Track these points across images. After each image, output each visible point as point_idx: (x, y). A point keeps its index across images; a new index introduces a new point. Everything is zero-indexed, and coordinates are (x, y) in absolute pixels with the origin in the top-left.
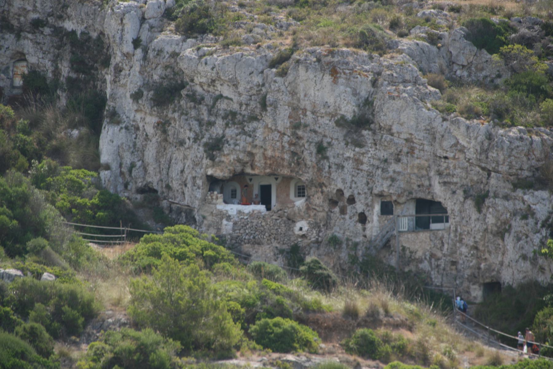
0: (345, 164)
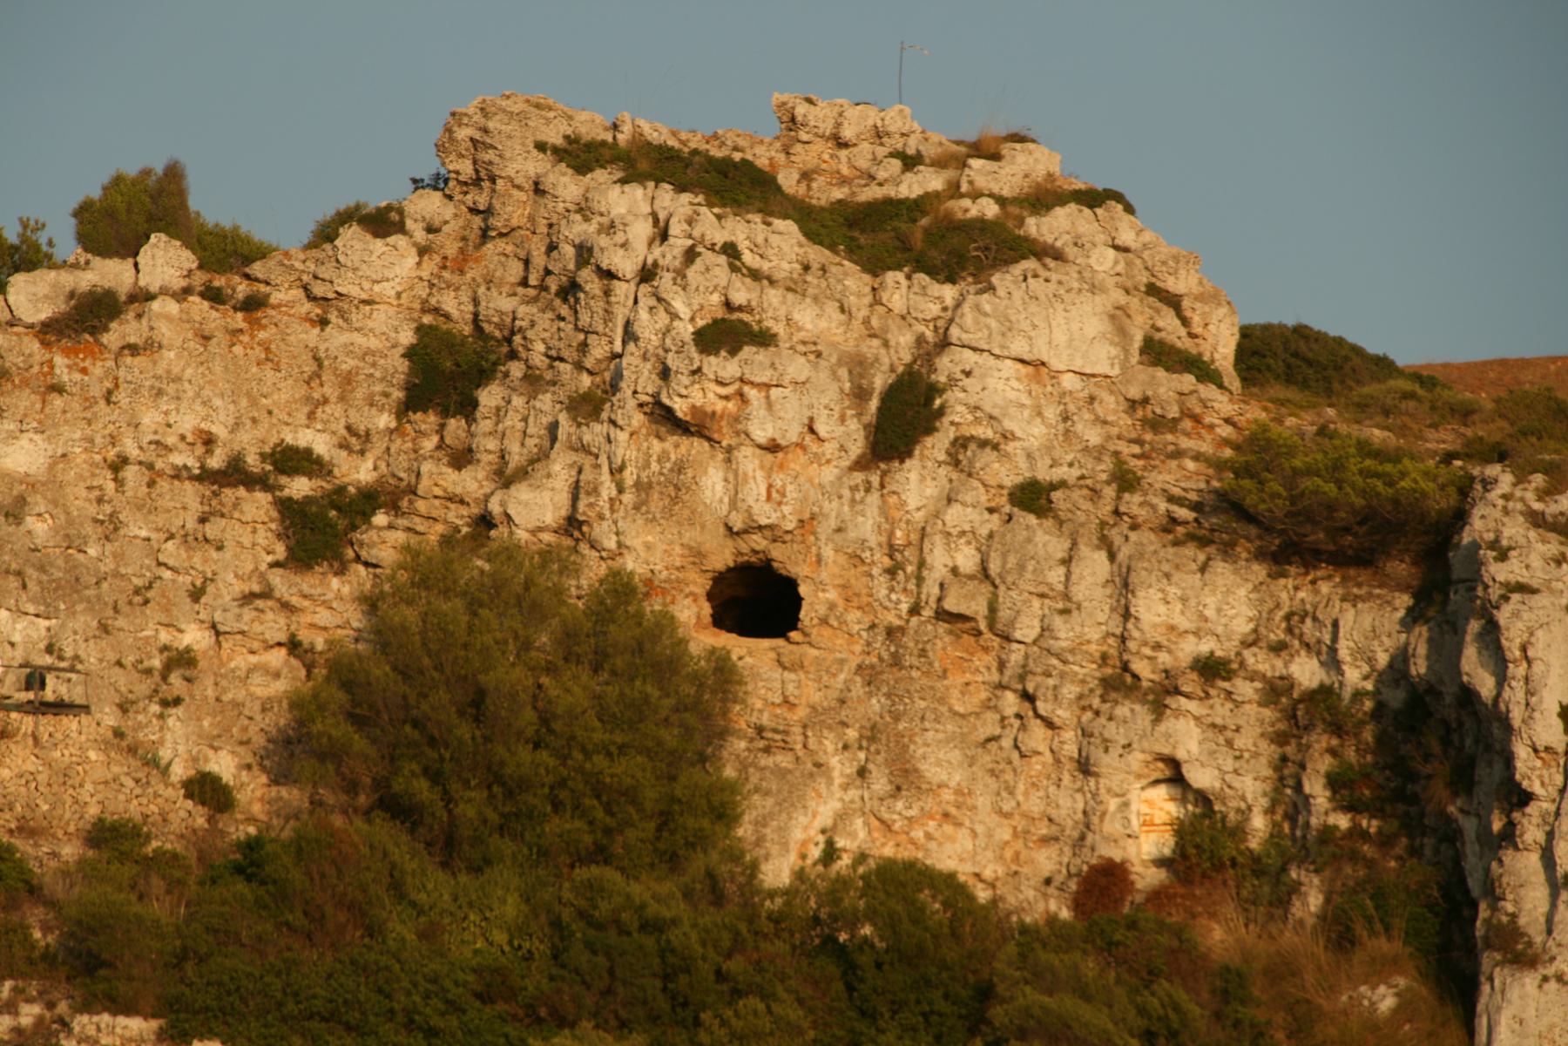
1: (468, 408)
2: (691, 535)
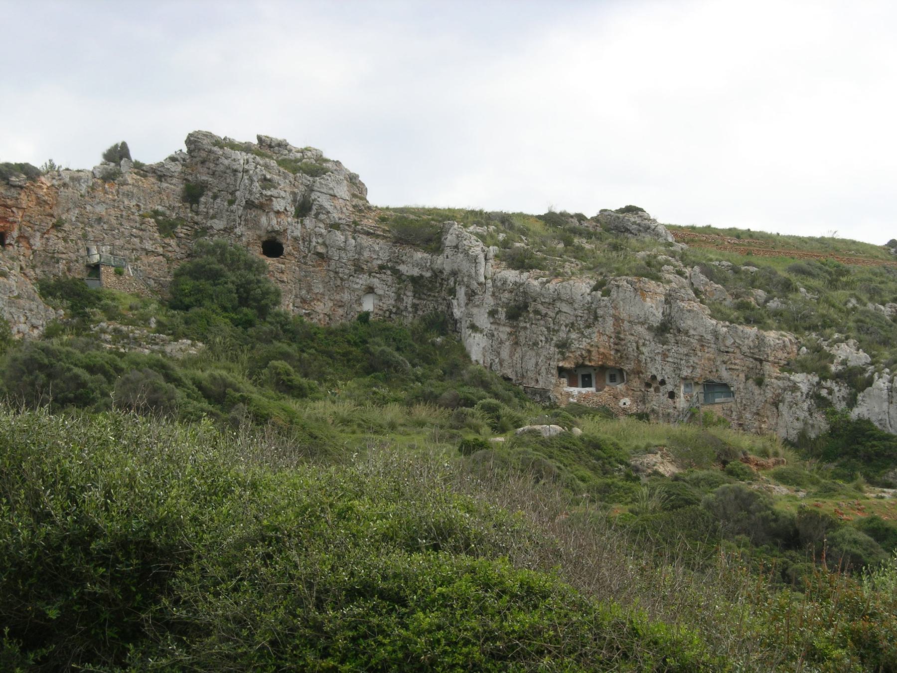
0: (657, 358)
1: (198, 202)
2: (258, 232)
